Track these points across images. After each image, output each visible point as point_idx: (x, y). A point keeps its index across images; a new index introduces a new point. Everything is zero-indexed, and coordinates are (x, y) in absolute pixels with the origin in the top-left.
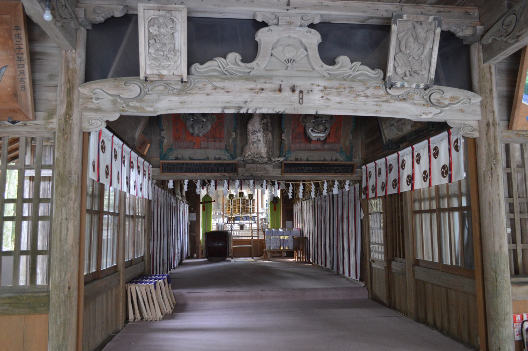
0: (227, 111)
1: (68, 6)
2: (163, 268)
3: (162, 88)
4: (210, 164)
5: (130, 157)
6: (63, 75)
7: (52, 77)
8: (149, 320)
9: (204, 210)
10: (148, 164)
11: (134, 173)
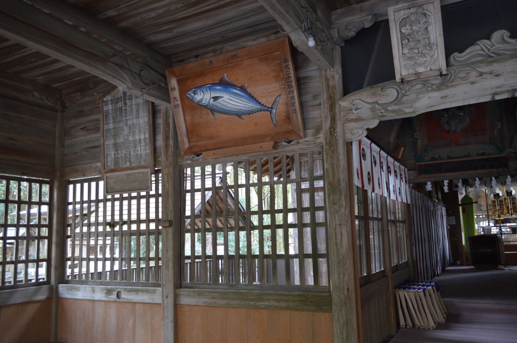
0: (497, 98)
1: (325, 30)
2: (427, 274)
3: (419, 86)
4: (473, 161)
5: (387, 162)
6: (325, 93)
7: (315, 97)
8: (421, 328)
9: (464, 212)
10: (404, 168)
11: (392, 178)
